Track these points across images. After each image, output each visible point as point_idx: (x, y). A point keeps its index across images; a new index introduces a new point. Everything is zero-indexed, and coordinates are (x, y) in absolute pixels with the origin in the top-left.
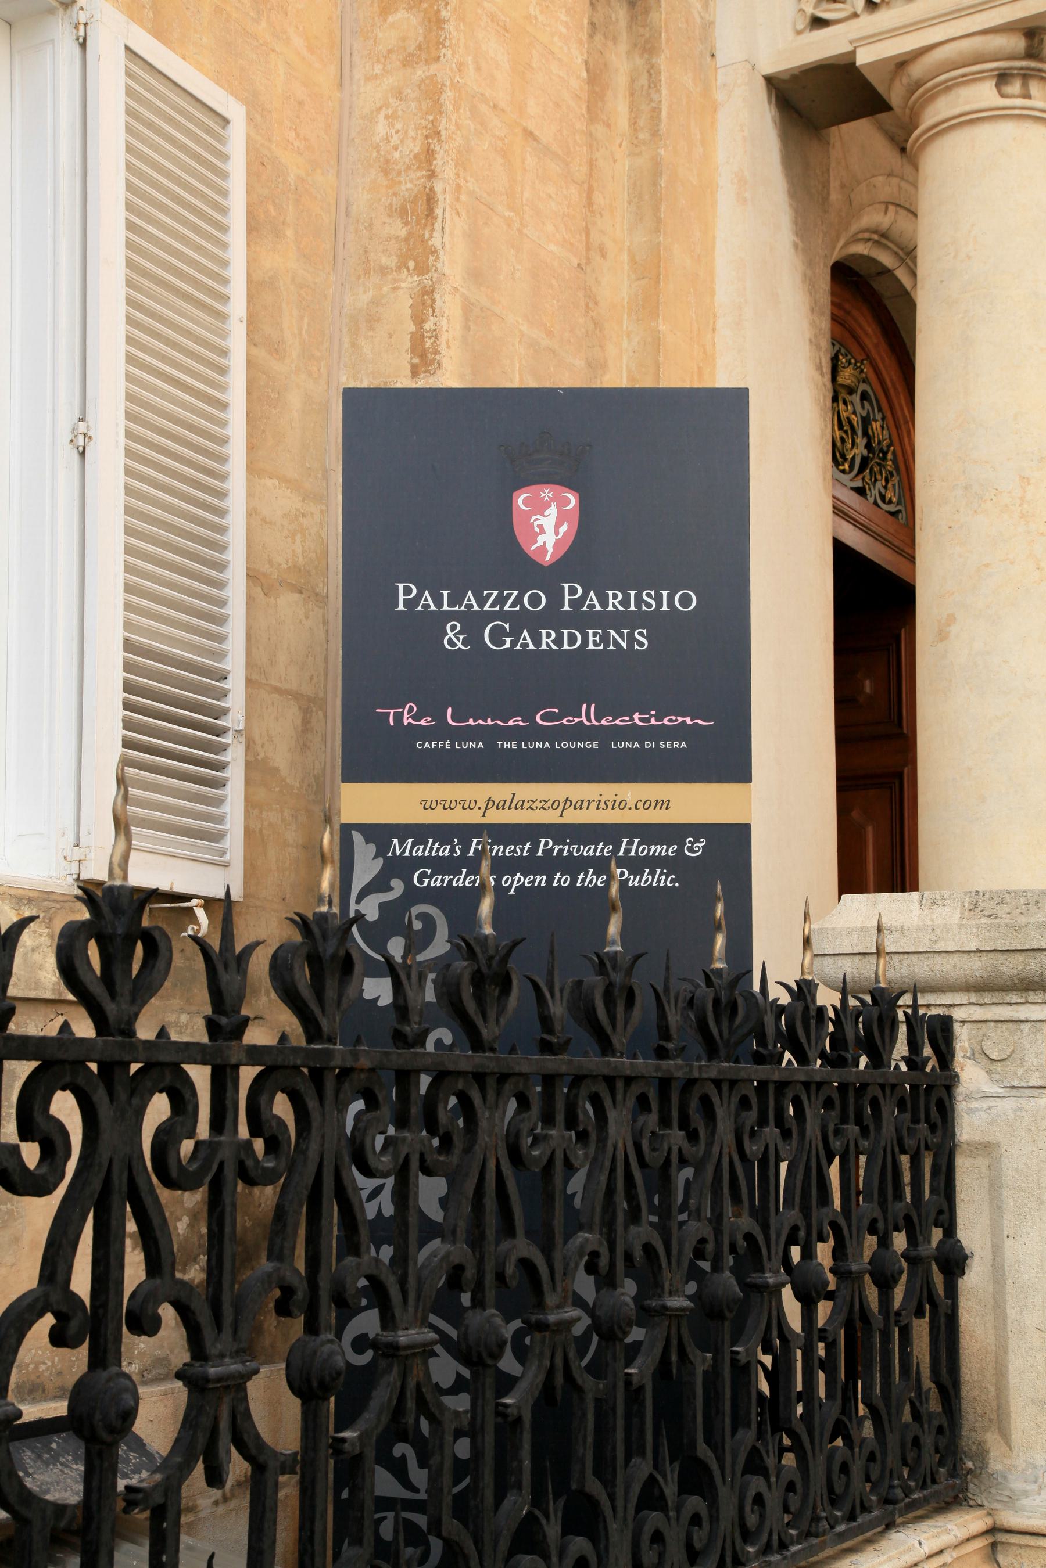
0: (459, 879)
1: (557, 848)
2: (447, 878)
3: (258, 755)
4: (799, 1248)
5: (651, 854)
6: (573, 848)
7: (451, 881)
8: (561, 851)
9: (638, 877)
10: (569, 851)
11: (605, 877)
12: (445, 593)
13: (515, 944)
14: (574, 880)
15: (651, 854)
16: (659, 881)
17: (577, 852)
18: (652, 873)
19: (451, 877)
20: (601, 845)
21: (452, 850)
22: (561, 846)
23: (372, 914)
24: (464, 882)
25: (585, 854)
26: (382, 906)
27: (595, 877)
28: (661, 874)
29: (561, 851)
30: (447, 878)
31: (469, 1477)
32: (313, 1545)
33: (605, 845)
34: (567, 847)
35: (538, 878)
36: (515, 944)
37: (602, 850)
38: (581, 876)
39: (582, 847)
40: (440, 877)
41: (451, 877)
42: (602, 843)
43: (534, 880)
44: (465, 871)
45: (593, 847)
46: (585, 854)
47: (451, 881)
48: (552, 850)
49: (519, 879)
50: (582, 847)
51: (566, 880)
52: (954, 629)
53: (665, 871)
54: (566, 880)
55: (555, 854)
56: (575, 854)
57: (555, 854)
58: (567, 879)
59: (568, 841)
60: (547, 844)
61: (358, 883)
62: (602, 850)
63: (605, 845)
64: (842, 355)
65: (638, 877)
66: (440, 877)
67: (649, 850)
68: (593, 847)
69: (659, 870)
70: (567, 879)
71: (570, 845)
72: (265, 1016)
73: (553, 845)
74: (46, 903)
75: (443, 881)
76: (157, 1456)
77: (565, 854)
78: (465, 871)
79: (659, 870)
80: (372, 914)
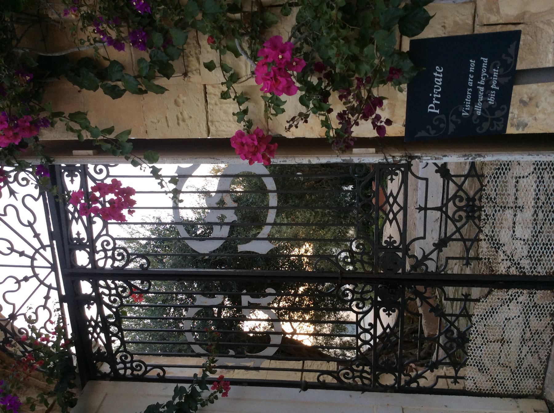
0: (485, 60)
1: (435, 102)
2: (470, 80)
4: (74, 347)
6: (436, 91)
8: (437, 99)
10: (437, 94)
13: (424, 168)
17: (439, 89)
20: (436, 74)
22: (434, 99)
23: (434, 132)
25: (441, 84)
26: (432, 129)
29: (437, 99)
30: (470, 80)
32: (266, 105)
33: (435, 71)
34: (435, 95)
36: (424, 168)
37: (439, 73)
39: (435, 86)
42: (434, 74)
45: (436, 79)
48: (436, 104)
50: (435, 86)
52: (447, 157)
55: (439, 102)
56: (440, 90)
57: (439, 102)
59: (431, 95)
60: (432, 108)
62: (439, 73)
63: (435, 71)
66: (469, 83)
68: (436, 79)
71: (433, 93)
73: (433, 104)
77: (439, 96)
80: (434, 132)
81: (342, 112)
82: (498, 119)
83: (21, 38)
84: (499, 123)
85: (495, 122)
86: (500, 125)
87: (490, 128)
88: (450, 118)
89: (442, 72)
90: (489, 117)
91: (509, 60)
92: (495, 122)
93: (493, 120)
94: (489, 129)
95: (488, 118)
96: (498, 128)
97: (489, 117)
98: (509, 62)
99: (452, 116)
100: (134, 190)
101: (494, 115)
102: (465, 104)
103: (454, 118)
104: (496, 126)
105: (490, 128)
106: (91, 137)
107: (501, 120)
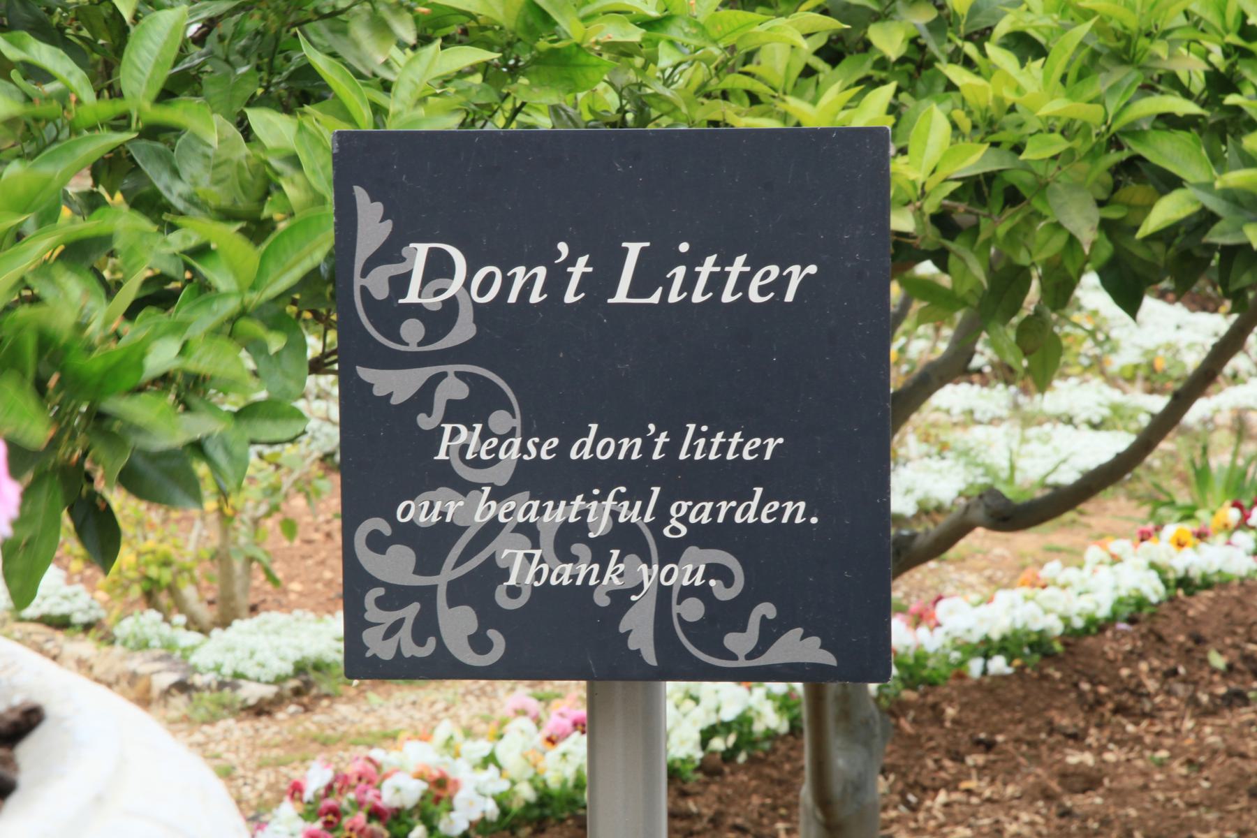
0: (747, 509)
2: (724, 506)
5: (513, 298)
7: (732, 512)
9: (638, 504)
12: (634, 249)
15: (513, 298)
19: (733, 504)
20: (738, 266)
21: (648, 446)
24: (758, 514)
28: (698, 434)
35: (789, 506)
37: (740, 448)
40: (709, 506)
41: (733, 504)
43: (781, 511)
47: (732, 512)
51: (405, 513)
53: (704, 428)
54: (405, 513)
59: (596, 492)
62: (740, 448)
64: (690, 48)
65: (638, 504)
69: (692, 427)
75: (715, 513)
76: (1108, 66)
78: (759, 491)
79: (692, 427)
81: (368, 654)
82: (426, 627)
83: (246, 131)
84: (405, 633)
85: (411, 611)
86: (392, 642)
87: (380, 592)
88: (451, 369)
89: (741, 457)
90: (441, 581)
91: (740, 643)
92: (411, 611)
93: (426, 596)
94: (376, 583)
95: (436, 571)
96: (380, 631)
97: (441, 581)
98: (732, 641)
99: (461, 376)
100: (1207, 74)
101: (452, 603)
102: (548, 256)
103: (453, 389)
104: (390, 617)
105: (380, 592)
106: (743, 629)
107: (419, 640)
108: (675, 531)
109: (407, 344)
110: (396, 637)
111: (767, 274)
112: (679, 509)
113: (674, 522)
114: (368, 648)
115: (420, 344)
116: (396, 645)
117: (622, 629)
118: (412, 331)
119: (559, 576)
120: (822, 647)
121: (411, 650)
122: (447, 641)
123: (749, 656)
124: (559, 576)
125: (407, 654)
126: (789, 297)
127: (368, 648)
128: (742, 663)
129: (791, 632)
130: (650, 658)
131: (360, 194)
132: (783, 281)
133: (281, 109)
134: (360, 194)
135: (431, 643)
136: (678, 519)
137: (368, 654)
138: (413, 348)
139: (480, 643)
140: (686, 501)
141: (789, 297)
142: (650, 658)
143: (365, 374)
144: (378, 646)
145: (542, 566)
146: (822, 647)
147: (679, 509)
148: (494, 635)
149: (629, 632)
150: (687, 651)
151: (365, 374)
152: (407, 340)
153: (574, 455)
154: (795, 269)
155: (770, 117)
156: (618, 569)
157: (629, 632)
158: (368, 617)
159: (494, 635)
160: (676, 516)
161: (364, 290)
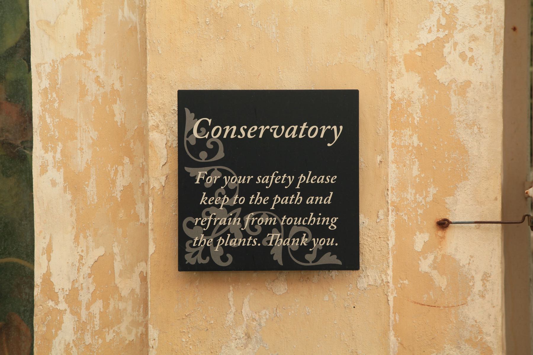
3: (419, 86)
6: (274, 129)
11: (268, 198)
14: (248, 200)
16: (228, 243)
17: (278, 134)
18: (316, 216)
20: (304, 126)
22: (329, 127)
27: (261, 198)
31: (186, 109)
38: (252, 197)
39: (283, 128)
40: (313, 198)
44: (310, 172)
46: (287, 136)
49: (278, 199)
50: (283, 128)
56: (275, 136)
58: (243, 199)
61: (383, 237)
66: (313, 198)
67: (223, 131)
70: (243, 199)
72: (388, 26)
74: (340, 328)
81: (187, 263)
84: (199, 255)
88: (216, 168)
107: (204, 258)
108: (332, 227)
109: (201, 160)
110: (196, 257)
111: (254, 129)
112: (334, 220)
113: (332, 225)
114: (187, 261)
115: (206, 159)
116: (196, 259)
117: (271, 253)
118: (203, 155)
119: (296, 242)
120: (337, 258)
121: (201, 261)
122: (213, 257)
123: (313, 262)
124: (296, 242)
125: (200, 263)
126: (261, 136)
127: (187, 261)
128: (311, 264)
129: (327, 253)
130: (281, 263)
131: (187, 110)
132: (259, 131)
133: (30, 73)
134: (187, 110)
135: (208, 258)
136: (333, 223)
137: (187, 263)
138: (203, 161)
139: (224, 258)
140: (336, 218)
141: (261, 136)
142: (281, 263)
143: (187, 169)
144: (190, 260)
145: (280, 239)
146: (337, 258)
147: (334, 220)
148: (228, 255)
149: (274, 254)
150: (292, 259)
151: (187, 169)
152: (201, 158)
153: (307, 203)
154: (263, 127)
155: (27, 63)
156: (305, 240)
157: (274, 254)
158: (187, 250)
159: (228, 255)
160: (333, 222)
161: (188, 142)
